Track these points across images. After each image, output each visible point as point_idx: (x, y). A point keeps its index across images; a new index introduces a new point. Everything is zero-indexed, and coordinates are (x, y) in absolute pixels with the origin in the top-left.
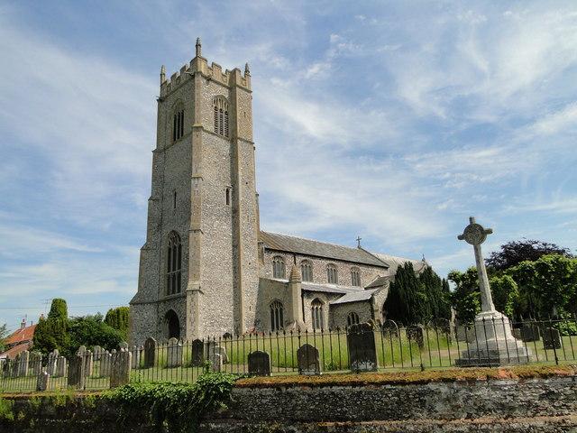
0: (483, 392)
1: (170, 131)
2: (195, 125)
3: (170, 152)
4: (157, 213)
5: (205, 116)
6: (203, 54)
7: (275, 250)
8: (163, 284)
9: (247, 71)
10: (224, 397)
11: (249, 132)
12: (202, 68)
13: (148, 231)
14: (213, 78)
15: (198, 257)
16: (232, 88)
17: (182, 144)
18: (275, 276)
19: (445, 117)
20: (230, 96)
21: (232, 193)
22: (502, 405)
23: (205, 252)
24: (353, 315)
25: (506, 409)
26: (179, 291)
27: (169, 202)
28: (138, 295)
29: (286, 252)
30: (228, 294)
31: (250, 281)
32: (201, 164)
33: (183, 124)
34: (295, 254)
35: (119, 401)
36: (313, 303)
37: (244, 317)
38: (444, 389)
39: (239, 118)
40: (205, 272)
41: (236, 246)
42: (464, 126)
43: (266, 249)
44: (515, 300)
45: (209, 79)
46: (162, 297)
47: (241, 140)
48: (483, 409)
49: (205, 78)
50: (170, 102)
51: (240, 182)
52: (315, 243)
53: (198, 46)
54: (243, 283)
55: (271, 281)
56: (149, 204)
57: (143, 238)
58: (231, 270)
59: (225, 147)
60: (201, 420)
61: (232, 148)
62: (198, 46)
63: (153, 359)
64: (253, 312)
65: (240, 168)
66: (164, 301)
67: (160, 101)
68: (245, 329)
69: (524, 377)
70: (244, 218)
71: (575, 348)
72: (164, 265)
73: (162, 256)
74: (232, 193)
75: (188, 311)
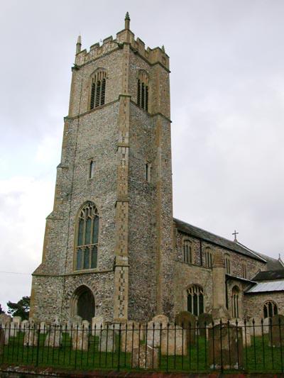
1: (86, 98)
22: (157, 216)
24: (270, 305)
26: (94, 265)
27: (82, 171)
28: (41, 267)
33: (103, 92)
46: (69, 270)
50: (88, 71)
53: (128, 19)
56: (58, 172)
62: (128, 19)
63: (187, 335)
66: (74, 276)
71: (282, 335)
73: (71, 227)
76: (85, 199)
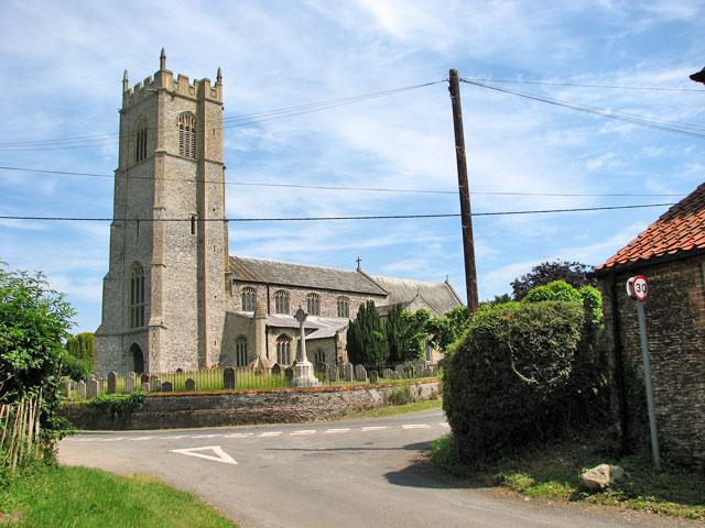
0: (242, 399)
1: (133, 150)
2: (159, 150)
3: (133, 173)
4: (119, 240)
5: (170, 139)
6: (168, 67)
7: (245, 278)
8: (127, 317)
9: (219, 77)
10: (141, 401)
11: (218, 151)
12: (167, 84)
13: (111, 260)
14: (178, 92)
15: (160, 292)
16: (200, 101)
17: (144, 167)
18: (244, 309)
19: (609, 6)
20: (198, 110)
21: (198, 221)
23: (166, 286)
24: (319, 351)
25: (251, 406)
26: (143, 324)
29: (258, 283)
30: (192, 329)
31: (215, 316)
32: (164, 193)
34: (268, 285)
35: (93, 405)
36: (278, 339)
37: (209, 352)
38: (227, 397)
39: (206, 136)
40: (167, 307)
41: (201, 278)
42: (642, 25)
43: (235, 281)
44: (459, 336)
45: (173, 95)
46: (126, 329)
47: (208, 161)
48: (241, 405)
49: (170, 93)
51: (206, 209)
52: (299, 267)
53: (163, 58)
54: (208, 318)
55: (238, 316)
57: (104, 266)
58: (196, 304)
59: (190, 169)
60: (132, 411)
61: (198, 169)
62: (163, 58)
64: (218, 347)
65: (207, 193)
67: (123, 112)
68: (209, 364)
69: (258, 393)
70: (210, 248)
72: (127, 296)
74: (198, 221)
75: (150, 347)
76: (134, 259)
